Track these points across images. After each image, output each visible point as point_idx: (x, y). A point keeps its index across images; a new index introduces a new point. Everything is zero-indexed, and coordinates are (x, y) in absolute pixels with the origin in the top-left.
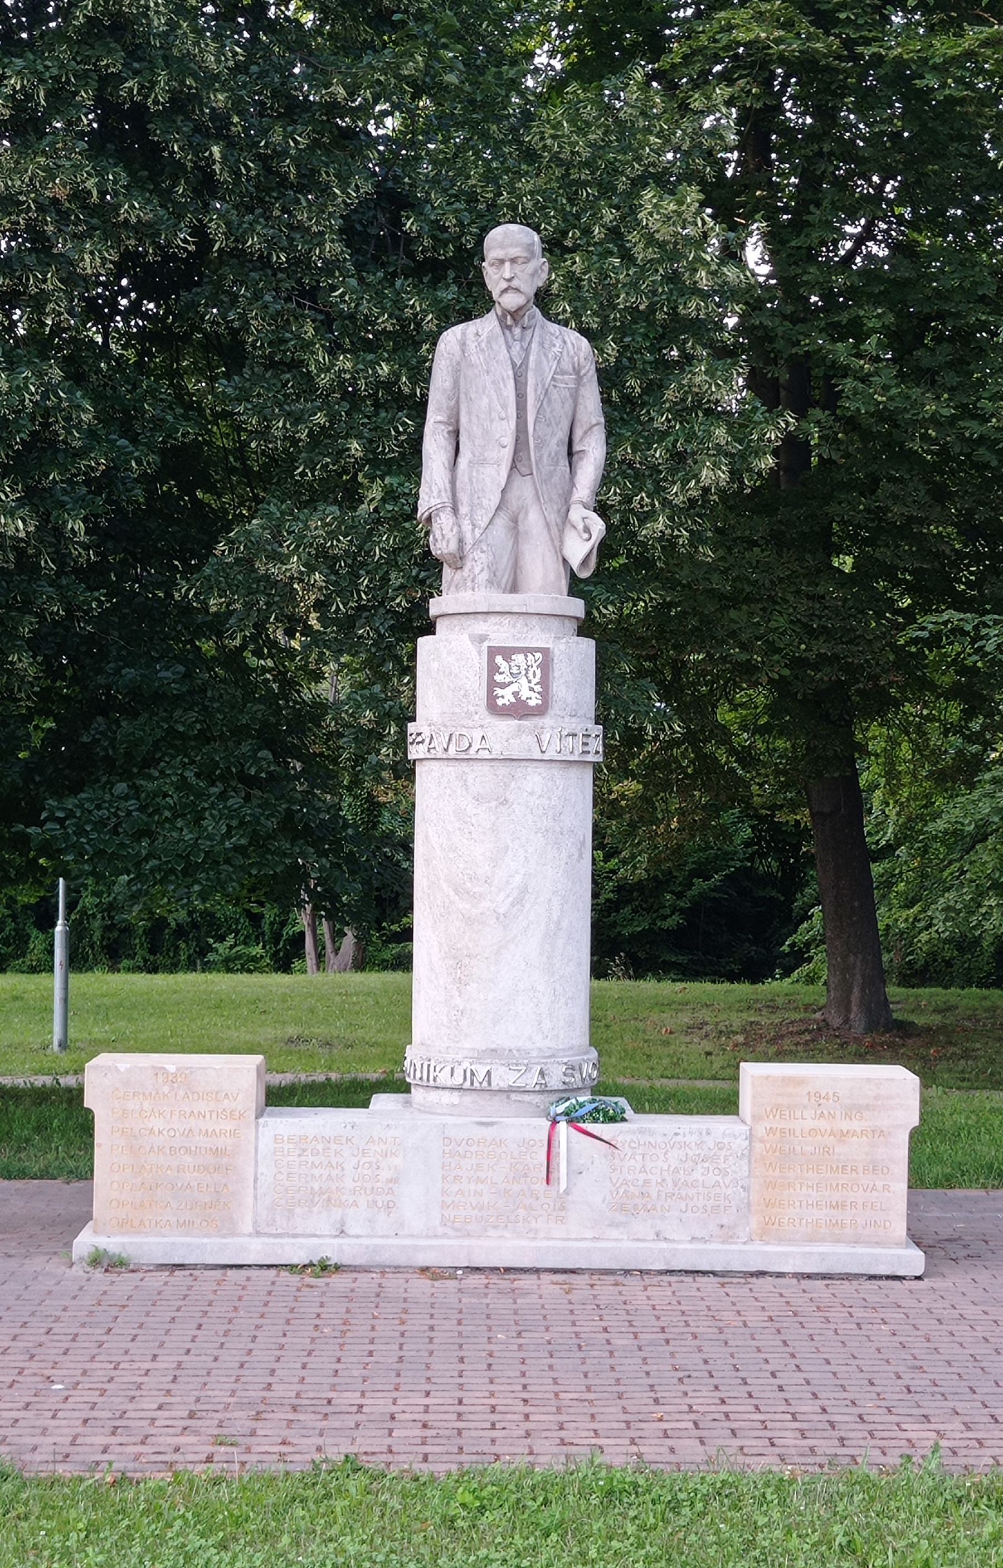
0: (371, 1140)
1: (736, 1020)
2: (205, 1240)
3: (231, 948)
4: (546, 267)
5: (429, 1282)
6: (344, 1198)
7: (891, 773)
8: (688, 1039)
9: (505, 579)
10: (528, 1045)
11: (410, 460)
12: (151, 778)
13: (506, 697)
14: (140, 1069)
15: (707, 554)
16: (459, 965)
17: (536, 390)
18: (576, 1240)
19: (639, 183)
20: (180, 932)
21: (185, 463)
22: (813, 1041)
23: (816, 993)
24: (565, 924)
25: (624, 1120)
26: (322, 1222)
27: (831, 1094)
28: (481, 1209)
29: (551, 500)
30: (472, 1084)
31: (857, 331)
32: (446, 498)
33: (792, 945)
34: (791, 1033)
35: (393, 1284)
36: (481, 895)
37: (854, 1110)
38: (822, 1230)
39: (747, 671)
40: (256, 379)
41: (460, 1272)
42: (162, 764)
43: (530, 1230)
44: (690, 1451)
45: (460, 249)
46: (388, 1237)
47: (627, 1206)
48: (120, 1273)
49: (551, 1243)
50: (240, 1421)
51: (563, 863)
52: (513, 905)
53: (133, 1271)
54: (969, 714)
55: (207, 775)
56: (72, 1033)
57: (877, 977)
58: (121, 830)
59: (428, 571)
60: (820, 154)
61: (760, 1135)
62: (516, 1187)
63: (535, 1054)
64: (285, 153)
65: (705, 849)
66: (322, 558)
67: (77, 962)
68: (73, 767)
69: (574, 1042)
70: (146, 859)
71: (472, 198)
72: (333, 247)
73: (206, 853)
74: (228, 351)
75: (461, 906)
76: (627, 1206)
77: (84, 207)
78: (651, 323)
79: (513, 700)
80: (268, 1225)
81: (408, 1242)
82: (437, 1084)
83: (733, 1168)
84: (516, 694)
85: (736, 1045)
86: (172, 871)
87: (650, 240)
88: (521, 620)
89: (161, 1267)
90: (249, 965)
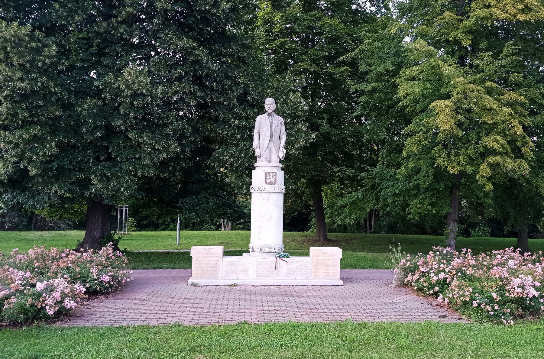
1: (300, 239)
7: (326, 195)
9: (269, 160)
11: (251, 139)
13: (269, 181)
15: (301, 156)
16: (260, 229)
19: (289, 92)
20: (198, 223)
21: (208, 140)
26: (234, 277)
31: (322, 119)
32: (258, 145)
35: (247, 288)
39: (303, 177)
40: (221, 124)
44: (306, 318)
45: (257, 102)
47: (289, 274)
50: (223, 315)
54: (341, 185)
55: (210, 195)
57: (325, 232)
59: (254, 158)
60: (316, 88)
64: (227, 85)
66: (233, 156)
67: (181, 229)
68: (185, 193)
71: (260, 93)
72: (235, 101)
74: (216, 120)
76: (289, 274)
77: (191, 93)
78: (291, 116)
87: (291, 102)
89: (204, 285)
90: (211, 229)
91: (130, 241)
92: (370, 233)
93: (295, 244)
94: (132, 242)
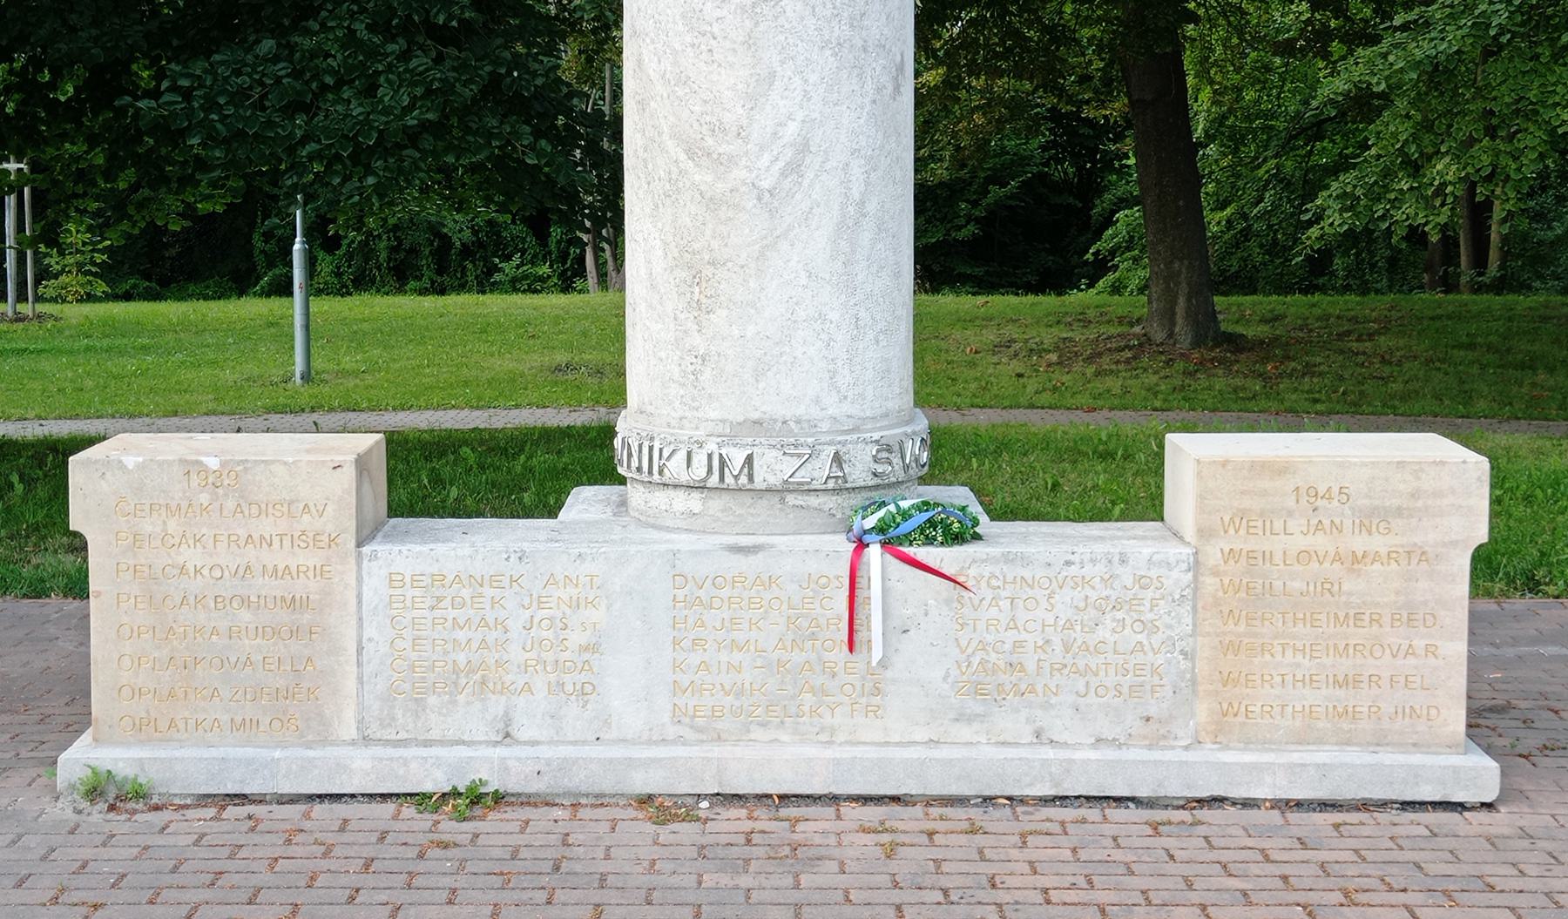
0: (551, 580)
1: (1049, 337)
2: (277, 754)
3: (518, 267)
5: (650, 828)
6: (508, 678)
8: (995, 359)
10: (815, 412)
12: (308, 32)
14: (161, 464)
16: (697, 279)
18: (898, 744)
20: (466, 251)
22: (1134, 358)
23: (1133, 304)
24: (871, 207)
25: (977, 537)
26: (473, 719)
27: (1335, 490)
28: (740, 694)
30: (722, 478)
33: (1097, 253)
34: (1109, 350)
36: (731, 158)
37: (1373, 517)
38: (1320, 725)
41: (704, 804)
42: (324, 14)
43: (823, 729)
46: (584, 743)
48: (135, 812)
49: (858, 751)
51: (867, 100)
52: (784, 174)
53: (157, 808)
56: (318, 364)
58: (267, 104)
61: (1211, 562)
62: (797, 657)
63: (825, 426)
65: (1000, 155)
69: (890, 405)
70: (304, 141)
73: (381, 132)
75: (697, 178)
76: (987, 686)
80: (383, 726)
81: (617, 752)
82: (666, 479)
83: (1167, 619)
85: (1049, 365)
86: (338, 157)
89: (205, 800)
90: (534, 286)
91: (26, 363)
92: (1478, 289)
93: (1017, 366)
94: (46, 364)
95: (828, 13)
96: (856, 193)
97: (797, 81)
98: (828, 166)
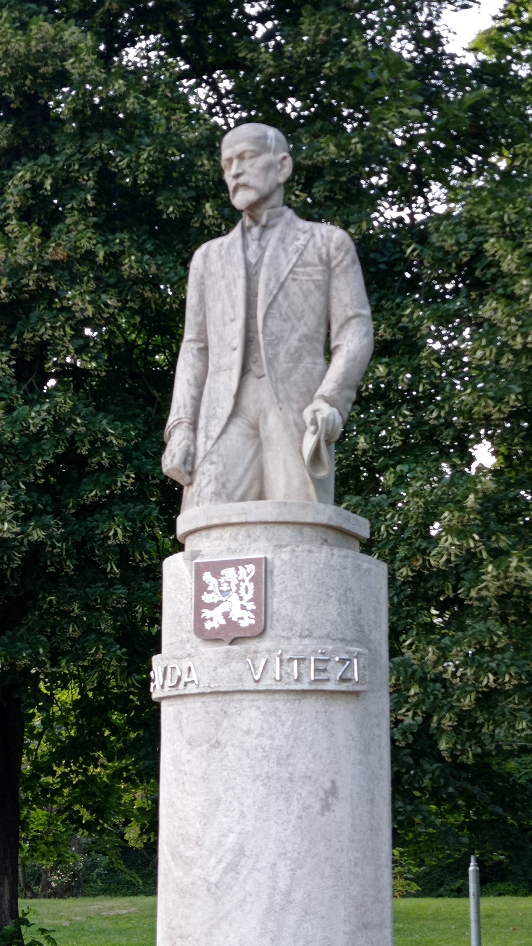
4: (227, 138)
13: (214, 619)
17: (267, 285)
29: (289, 399)
51: (293, 817)
52: (225, 872)
67: (482, 892)
79: (223, 622)
84: (226, 615)
88: (243, 531)
95: (259, 756)
96: (282, 886)
97: (236, 804)
98: (258, 866)
